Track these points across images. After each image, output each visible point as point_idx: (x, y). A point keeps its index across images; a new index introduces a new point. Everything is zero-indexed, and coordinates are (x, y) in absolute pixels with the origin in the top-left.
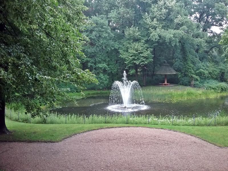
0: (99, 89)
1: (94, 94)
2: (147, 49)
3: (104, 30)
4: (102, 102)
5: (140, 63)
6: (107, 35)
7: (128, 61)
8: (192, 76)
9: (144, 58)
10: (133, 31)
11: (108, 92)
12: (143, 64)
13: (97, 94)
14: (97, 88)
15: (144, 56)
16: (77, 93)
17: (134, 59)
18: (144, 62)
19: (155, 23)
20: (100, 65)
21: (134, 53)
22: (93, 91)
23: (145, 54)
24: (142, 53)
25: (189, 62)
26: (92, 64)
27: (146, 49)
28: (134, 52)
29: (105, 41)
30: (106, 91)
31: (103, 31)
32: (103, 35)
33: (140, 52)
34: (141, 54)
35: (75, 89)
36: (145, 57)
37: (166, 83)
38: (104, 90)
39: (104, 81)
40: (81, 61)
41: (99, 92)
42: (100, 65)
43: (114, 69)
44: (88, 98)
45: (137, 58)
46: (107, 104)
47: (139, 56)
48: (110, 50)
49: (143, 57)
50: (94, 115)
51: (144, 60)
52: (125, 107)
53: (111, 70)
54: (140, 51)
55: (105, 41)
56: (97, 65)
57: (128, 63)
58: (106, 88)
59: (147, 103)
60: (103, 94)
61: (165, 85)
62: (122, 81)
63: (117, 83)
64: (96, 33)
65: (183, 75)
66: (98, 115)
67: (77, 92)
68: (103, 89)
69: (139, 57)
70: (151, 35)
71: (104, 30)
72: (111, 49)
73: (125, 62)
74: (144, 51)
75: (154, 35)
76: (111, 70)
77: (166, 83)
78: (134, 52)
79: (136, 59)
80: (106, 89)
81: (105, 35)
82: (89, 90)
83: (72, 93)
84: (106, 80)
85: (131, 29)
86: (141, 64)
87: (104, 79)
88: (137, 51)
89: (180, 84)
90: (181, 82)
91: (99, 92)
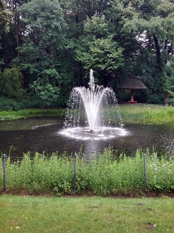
0: (47, 107)
1: (38, 113)
2: (117, 48)
3: (54, 16)
4: (48, 124)
5: (107, 68)
6: (58, 24)
7: (89, 65)
8: (167, 92)
9: (113, 61)
10: (98, 22)
11: (58, 111)
12: (111, 69)
13: (43, 113)
14: (43, 106)
15: (114, 57)
16: (13, 112)
17: (98, 62)
18: (112, 66)
19: (130, 10)
20: (48, 72)
21: (98, 53)
22: (37, 109)
23: (114, 55)
24: (110, 53)
25: (165, 73)
26: (35, 70)
27: (115, 48)
28: (99, 51)
29: (55, 34)
30: (55, 110)
31: (53, 18)
32: (53, 24)
33: (107, 51)
34: (108, 55)
35: (10, 106)
36: (114, 59)
37: (132, 100)
38: (52, 109)
39: (53, 94)
40: (21, 68)
41: (45, 111)
42: (48, 72)
43: (67, 80)
44: (29, 118)
45: (103, 60)
46: (61, 126)
47: (105, 57)
48: (62, 49)
49: (111, 58)
50: (37, 153)
51: (113, 63)
52: (91, 131)
53: (63, 80)
54: (107, 49)
55: (55, 34)
56: (43, 71)
57: (89, 68)
58: (56, 106)
59: (127, 126)
60: (50, 113)
61: (132, 103)
62: (87, 86)
63: (80, 90)
64: (42, 21)
65: (152, 92)
66: (48, 155)
67: (14, 110)
68: (51, 107)
69: (105, 59)
70: (125, 25)
71: (54, 16)
72: (64, 47)
73: (85, 67)
74: (113, 51)
75: (130, 25)
76: (63, 80)
77: (132, 100)
78: (99, 51)
79: (101, 61)
80: (55, 107)
81: (55, 23)
82: (31, 108)
83: (7, 111)
84: (55, 93)
85: (94, 17)
86: (107, 69)
87: (54, 92)
88: (103, 50)
89: (149, 103)
90: (149, 100)
91: (45, 111)
